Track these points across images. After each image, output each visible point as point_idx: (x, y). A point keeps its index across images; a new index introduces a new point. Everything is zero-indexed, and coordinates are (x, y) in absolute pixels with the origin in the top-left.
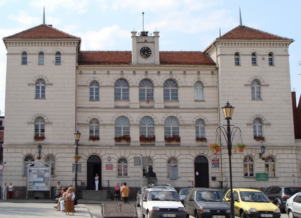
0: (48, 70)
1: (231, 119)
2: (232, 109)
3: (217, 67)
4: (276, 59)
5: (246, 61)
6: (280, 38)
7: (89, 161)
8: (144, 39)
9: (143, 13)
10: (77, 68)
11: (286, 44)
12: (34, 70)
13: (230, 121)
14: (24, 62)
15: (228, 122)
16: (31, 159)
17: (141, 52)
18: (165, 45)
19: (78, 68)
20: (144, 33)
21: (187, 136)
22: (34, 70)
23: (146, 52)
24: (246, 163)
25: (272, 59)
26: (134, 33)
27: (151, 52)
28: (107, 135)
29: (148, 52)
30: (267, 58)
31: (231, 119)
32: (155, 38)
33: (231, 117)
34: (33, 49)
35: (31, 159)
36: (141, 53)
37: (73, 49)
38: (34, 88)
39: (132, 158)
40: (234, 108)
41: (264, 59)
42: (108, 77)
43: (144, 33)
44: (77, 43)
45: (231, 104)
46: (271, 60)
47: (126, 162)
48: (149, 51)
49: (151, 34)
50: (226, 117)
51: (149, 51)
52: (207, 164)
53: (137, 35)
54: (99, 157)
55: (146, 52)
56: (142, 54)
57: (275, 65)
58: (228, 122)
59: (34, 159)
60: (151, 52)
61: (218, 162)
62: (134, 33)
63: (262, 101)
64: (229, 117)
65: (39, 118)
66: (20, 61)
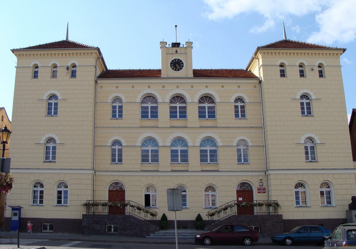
0: (62, 86)
1: (7, 144)
2: (9, 133)
3: (260, 80)
4: (327, 71)
5: (292, 72)
6: (329, 49)
7: (111, 189)
8: (175, 49)
9: (176, 26)
10: (96, 82)
11: (337, 54)
12: (46, 86)
13: (6, 145)
14: (36, 75)
15: (4, 146)
16: (298, 187)
17: (171, 65)
18: (200, 61)
19: (97, 82)
20: (174, 46)
21: (227, 158)
22: (46, 86)
23: (177, 65)
24: (35, 189)
25: (321, 71)
26: (163, 44)
27: (182, 65)
28: (132, 158)
29: (179, 66)
30: (317, 69)
31: (7, 144)
32: (188, 49)
33: (7, 141)
34: (46, 61)
35: (298, 187)
36: (171, 66)
37: (91, 60)
38: (43, 150)
39: (317, 184)
40: (11, 132)
41: (313, 70)
42: (132, 93)
43: (174, 46)
44: (95, 53)
45: (9, 128)
46: (321, 72)
47: (214, 191)
48: (180, 63)
49: (183, 43)
50: (2, 141)
51: (180, 63)
52: (252, 191)
53: (167, 46)
54: (250, 185)
55: (177, 65)
56: (173, 67)
57: (288, 76)
58: (4, 146)
59: (43, 186)
60: (182, 65)
61: (264, 191)
62: (163, 44)
63: (247, 120)
64: (5, 141)
65: (51, 140)
66: (50, 74)
